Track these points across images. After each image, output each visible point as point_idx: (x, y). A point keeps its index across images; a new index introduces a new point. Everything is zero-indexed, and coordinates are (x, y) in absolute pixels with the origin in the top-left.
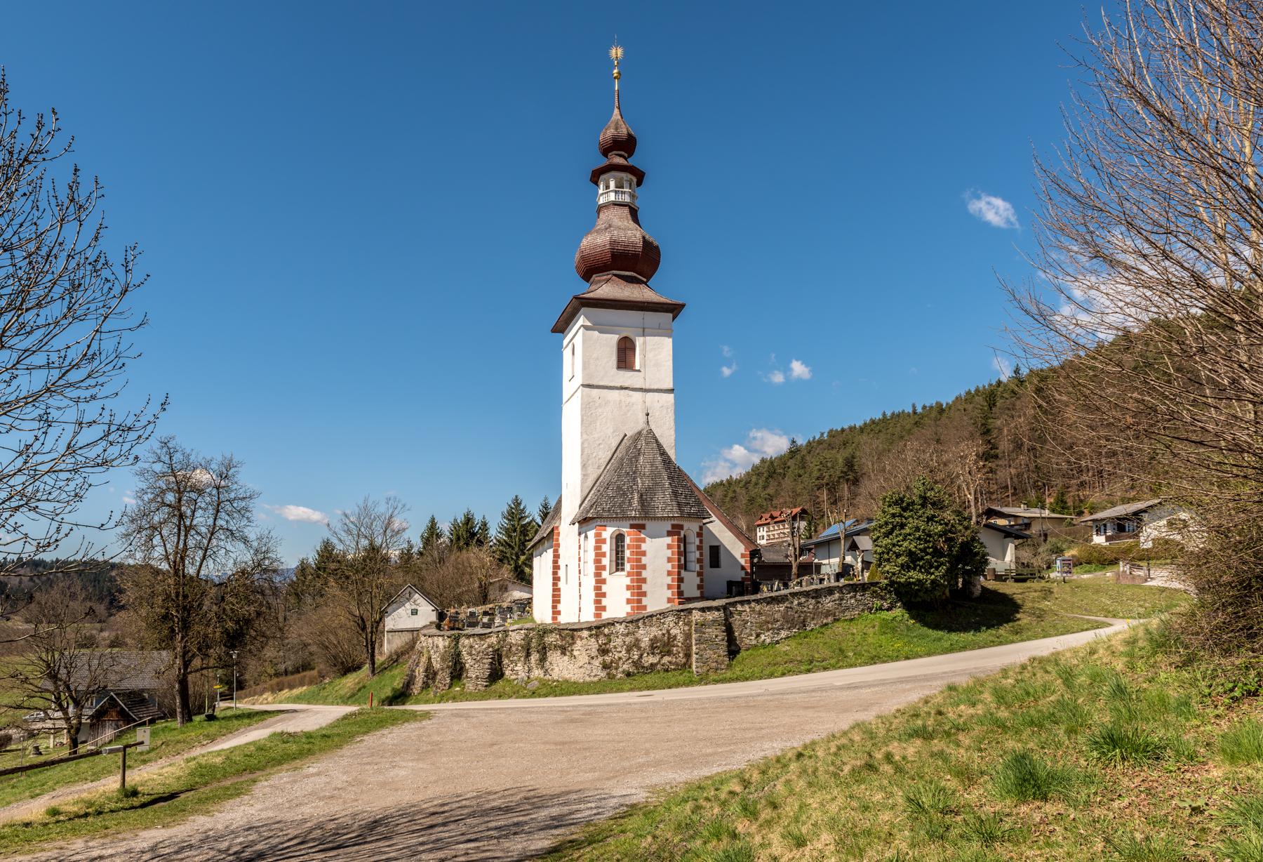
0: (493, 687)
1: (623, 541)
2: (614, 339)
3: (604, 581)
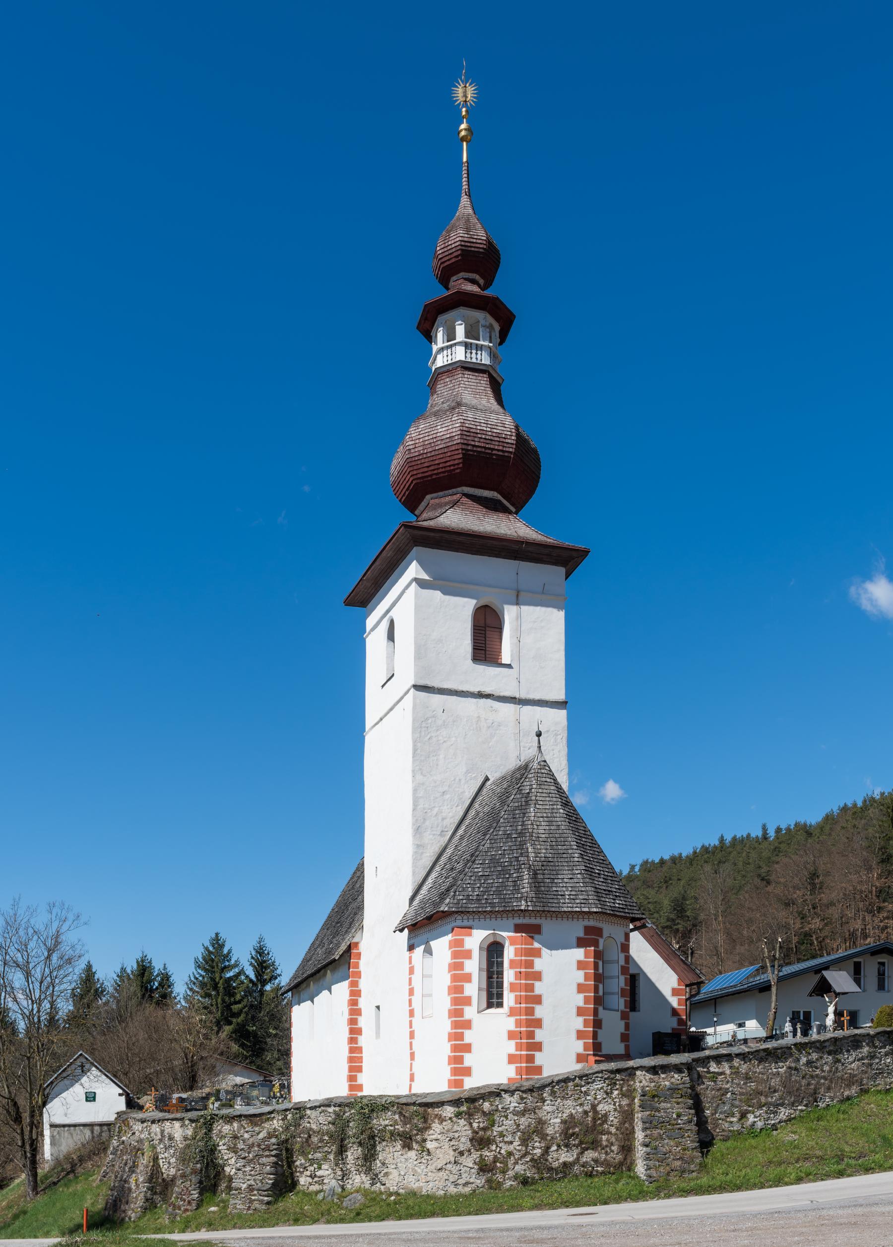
0: (281, 1205)
1: (501, 955)
2: (466, 607)
3: (468, 1025)
